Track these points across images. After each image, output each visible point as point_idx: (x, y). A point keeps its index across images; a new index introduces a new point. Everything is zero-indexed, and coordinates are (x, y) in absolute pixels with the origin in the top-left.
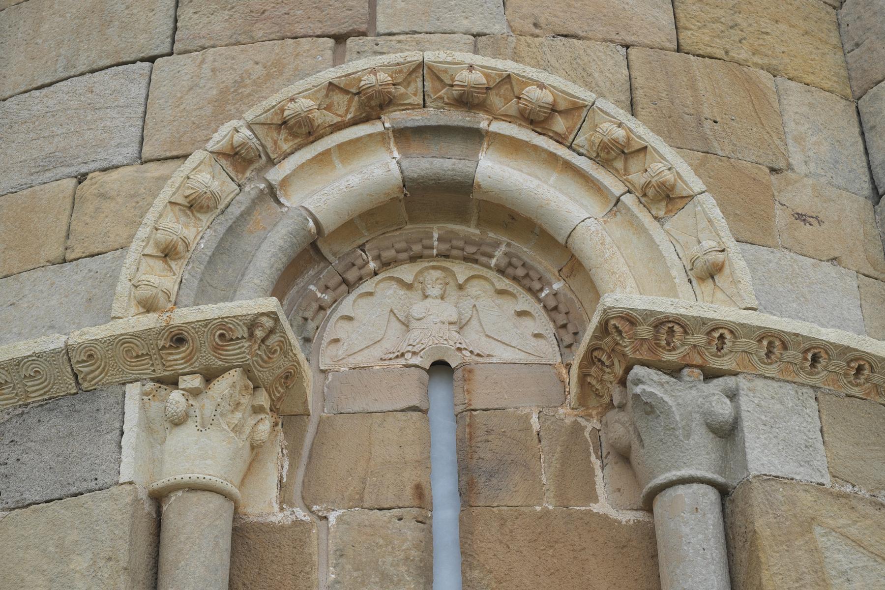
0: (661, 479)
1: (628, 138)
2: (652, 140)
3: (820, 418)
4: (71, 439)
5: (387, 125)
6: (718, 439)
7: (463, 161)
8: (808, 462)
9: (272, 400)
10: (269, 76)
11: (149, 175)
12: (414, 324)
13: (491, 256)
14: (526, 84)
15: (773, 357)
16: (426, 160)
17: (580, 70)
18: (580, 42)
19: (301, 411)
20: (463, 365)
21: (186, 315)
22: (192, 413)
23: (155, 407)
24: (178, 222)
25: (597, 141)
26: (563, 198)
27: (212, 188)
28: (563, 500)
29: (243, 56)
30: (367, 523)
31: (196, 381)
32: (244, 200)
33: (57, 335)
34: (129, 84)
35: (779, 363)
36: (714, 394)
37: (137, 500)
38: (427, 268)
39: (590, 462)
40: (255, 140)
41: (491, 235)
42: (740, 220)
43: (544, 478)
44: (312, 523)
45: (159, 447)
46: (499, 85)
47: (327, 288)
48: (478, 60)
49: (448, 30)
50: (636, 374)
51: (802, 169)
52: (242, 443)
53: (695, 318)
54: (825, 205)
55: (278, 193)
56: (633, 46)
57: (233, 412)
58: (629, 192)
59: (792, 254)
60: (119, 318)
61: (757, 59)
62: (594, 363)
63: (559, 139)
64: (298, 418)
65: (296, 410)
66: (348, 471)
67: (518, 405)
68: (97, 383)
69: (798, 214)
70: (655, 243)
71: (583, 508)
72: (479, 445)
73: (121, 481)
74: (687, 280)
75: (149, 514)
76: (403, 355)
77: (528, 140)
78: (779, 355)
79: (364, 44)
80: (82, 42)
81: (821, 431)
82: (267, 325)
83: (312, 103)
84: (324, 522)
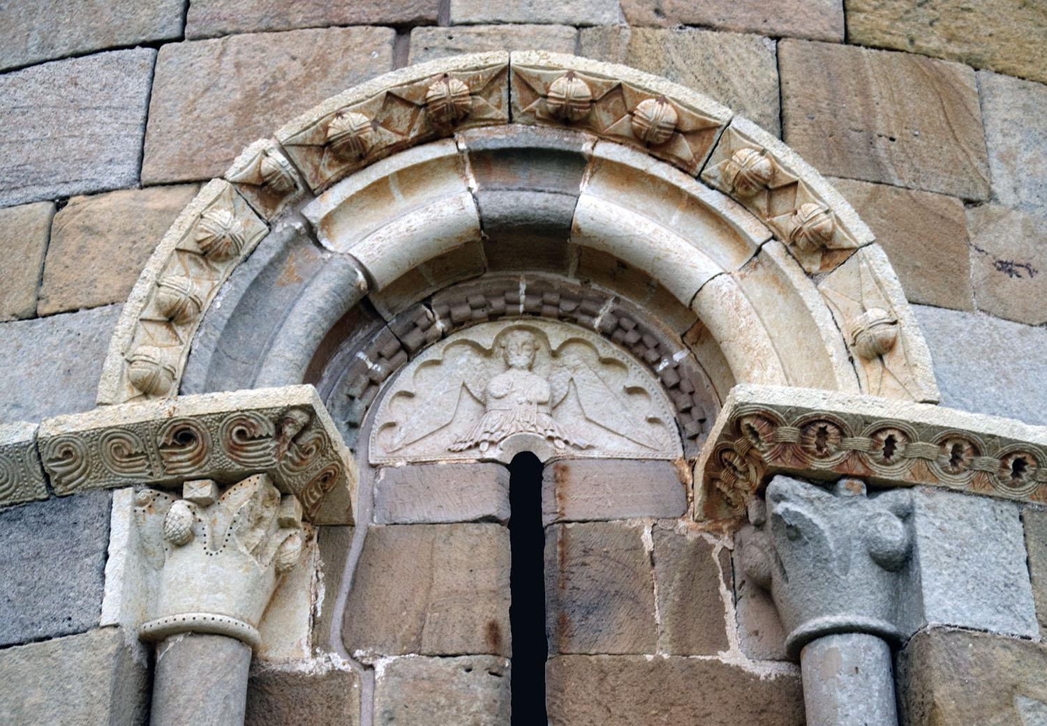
0: (809, 626)
1: (774, 170)
2: (804, 173)
3: (1026, 545)
4: (37, 563)
5: (462, 146)
6: (886, 573)
7: (559, 196)
8: (1009, 607)
9: (305, 508)
10: (309, 77)
11: (149, 205)
12: (493, 404)
13: (594, 315)
14: (643, 97)
15: (960, 465)
16: (510, 194)
17: (714, 74)
18: (716, 34)
19: (343, 520)
20: (555, 460)
21: (195, 405)
22: (199, 530)
23: (151, 520)
24: (187, 275)
25: (733, 173)
26: (687, 247)
27: (233, 231)
28: (682, 646)
29: (276, 48)
30: (425, 675)
31: (204, 490)
32: (274, 243)
33: (24, 423)
34: (125, 78)
35: (968, 472)
36: (880, 514)
37: (123, 649)
38: (511, 329)
39: (719, 594)
40: (290, 167)
41: (595, 286)
42: (921, 275)
43: (657, 616)
44: (352, 675)
45: (154, 573)
46: (607, 97)
47: (380, 356)
48: (581, 63)
49: (543, 19)
50: (777, 488)
51: (1009, 199)
52: (264, 568)
53: (855, 416)
54: (1039, 247)
55: (319, 233)
56: (786, 37)
57: (253, 529)
58: (774, 238)
59: (991, 319)
60: (106, 404)
61: (953, 48)
62: (724, 467)
63: (685, 167)
64: (339, 530)
65: (336, 519)
66: (402, 603)
67: (626, 516)
68: (75, 487)
69: (1001, 262)
70: (807, 309)
71: (708, 658)
72: (574, 569)
73: (103, 624)
74: (847, 358)
75: (139, 664)
76: (477, 445)
77: (643, 168)
78: (968, 463)
79: (434, 37)
80: (63, 12)
81: (1028, 562)
82: (300, 420)
83: (365, 119)
84: (369, 672)
